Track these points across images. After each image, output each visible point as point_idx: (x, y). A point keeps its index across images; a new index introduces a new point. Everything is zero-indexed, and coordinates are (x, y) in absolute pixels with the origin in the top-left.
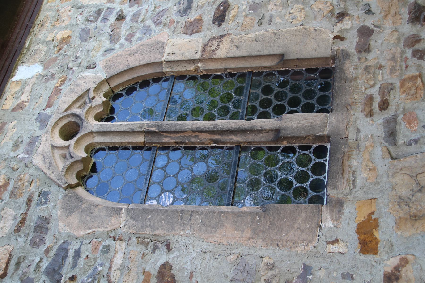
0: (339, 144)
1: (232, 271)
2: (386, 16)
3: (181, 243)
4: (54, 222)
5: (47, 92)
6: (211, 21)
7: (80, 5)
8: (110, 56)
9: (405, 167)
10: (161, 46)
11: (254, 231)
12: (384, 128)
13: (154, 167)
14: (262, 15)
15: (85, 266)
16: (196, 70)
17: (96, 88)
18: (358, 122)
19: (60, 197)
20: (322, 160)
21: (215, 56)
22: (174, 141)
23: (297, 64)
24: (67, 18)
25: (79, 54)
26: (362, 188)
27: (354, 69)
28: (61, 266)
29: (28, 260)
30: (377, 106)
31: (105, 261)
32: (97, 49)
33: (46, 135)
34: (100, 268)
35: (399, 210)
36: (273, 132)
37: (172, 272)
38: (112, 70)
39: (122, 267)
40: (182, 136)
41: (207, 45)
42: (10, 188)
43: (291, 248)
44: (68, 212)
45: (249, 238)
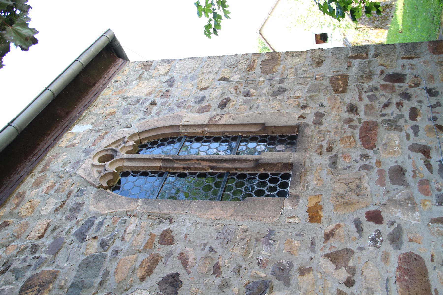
0: (299, 167)
1: (216, 234)
2: (333, 108)
3: (181, 219)
4: (86, 206)
5: (93, 138)
6: (217, 107)
7: (125, 97)
8: (142, 121)
9: (342, 179)
10: (181, 118)
11: (235, 211)
12: (329, 160)
13: (165, 182)
14: (252, 105)
15: (106, 231)
16: (203, 132)
17: (130, 137)
18: (312, 157)
19: (93, 192)
20: (287, 181)
21: (217, 123)
22: (183, 166)
23: (273, 131)
24: (115, 103)
25: (120, 120)
26: (312, 189)
27: (311, 132)
28: (87, 230)
29: (62, 227)
30: (325, 150)
31: (121, 229)
32: (134, 118)
33: (89, 159)
34: (116, 233)
35: (337, 201)
36: (254, 162)
37: (172, 234)
38: (144, 128)
39: (134, 232)
40: (189, 163)
41: (213, 118)
42: (55, 188)
43: (261, 220)
44: (97, 200)
45: (231, 215)
